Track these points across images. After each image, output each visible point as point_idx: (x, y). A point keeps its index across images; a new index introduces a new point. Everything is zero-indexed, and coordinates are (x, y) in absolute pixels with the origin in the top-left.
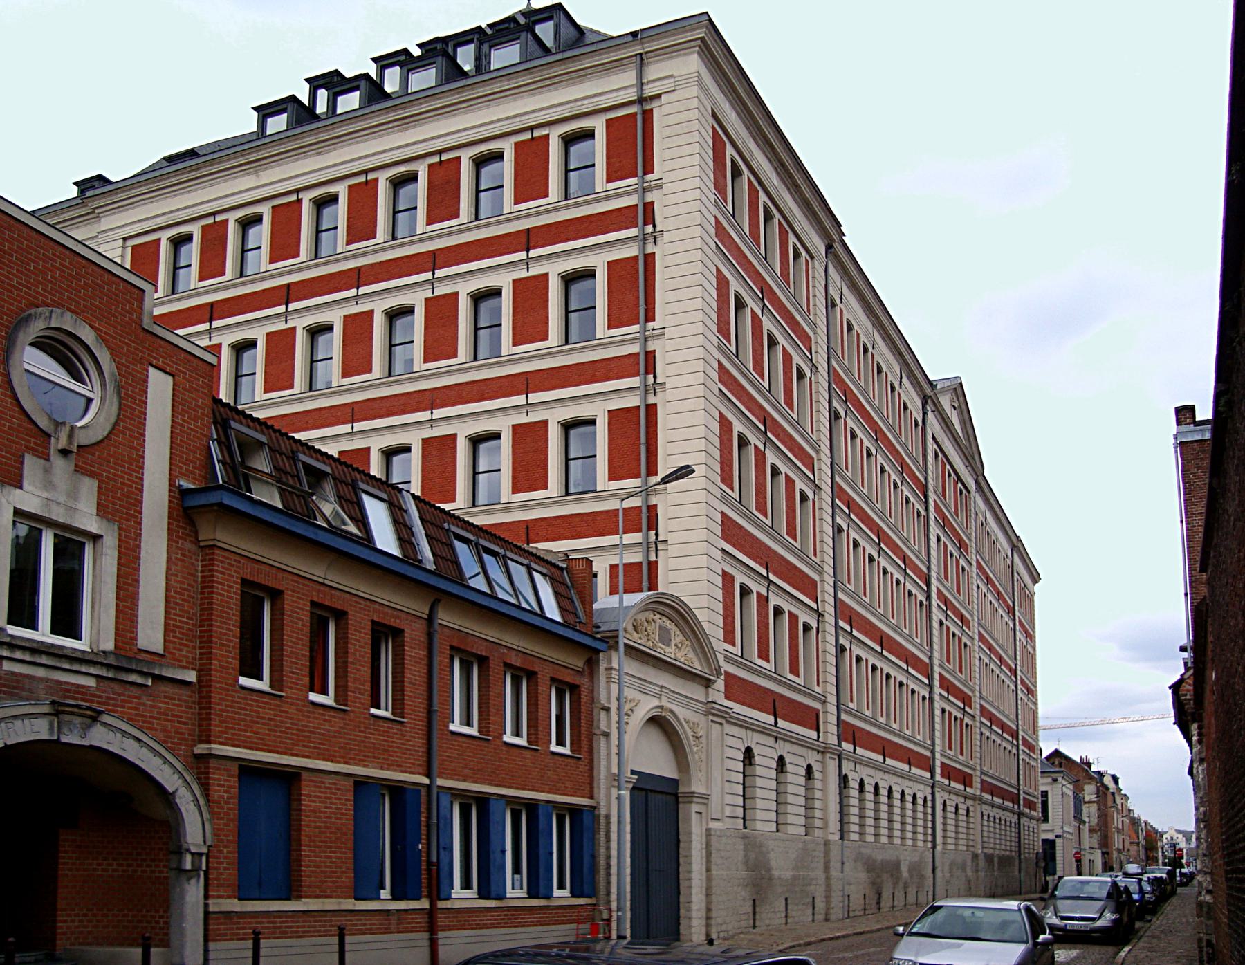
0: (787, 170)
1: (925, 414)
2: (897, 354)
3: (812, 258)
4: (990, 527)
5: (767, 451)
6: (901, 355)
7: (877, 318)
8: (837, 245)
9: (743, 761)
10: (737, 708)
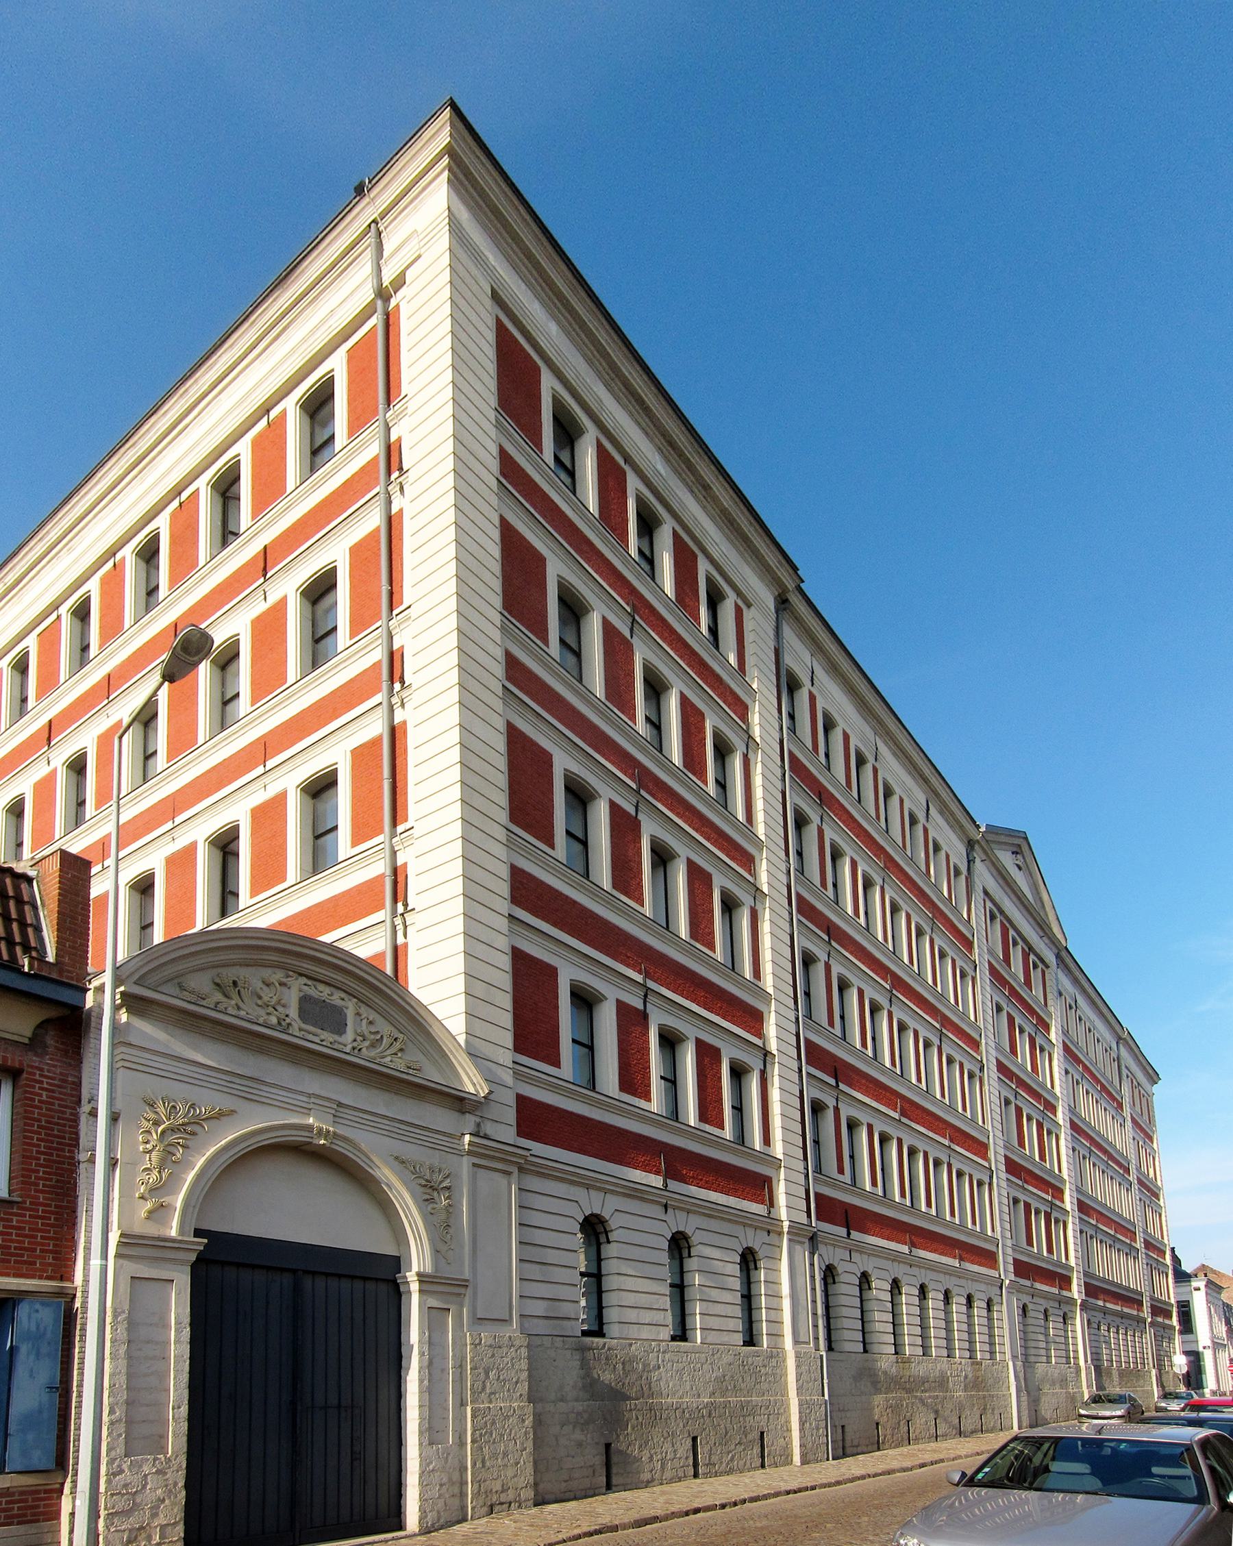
0: (681, 455)
1: (970, 862)
2: (917, 776)
3: (1047, 967)
4: (1099, 1032)
5: (641, 817)
6: (926, 780)
7: (880, 722)
8: (795, 599)
9: (891, 1291)
10: (538, 1148)
